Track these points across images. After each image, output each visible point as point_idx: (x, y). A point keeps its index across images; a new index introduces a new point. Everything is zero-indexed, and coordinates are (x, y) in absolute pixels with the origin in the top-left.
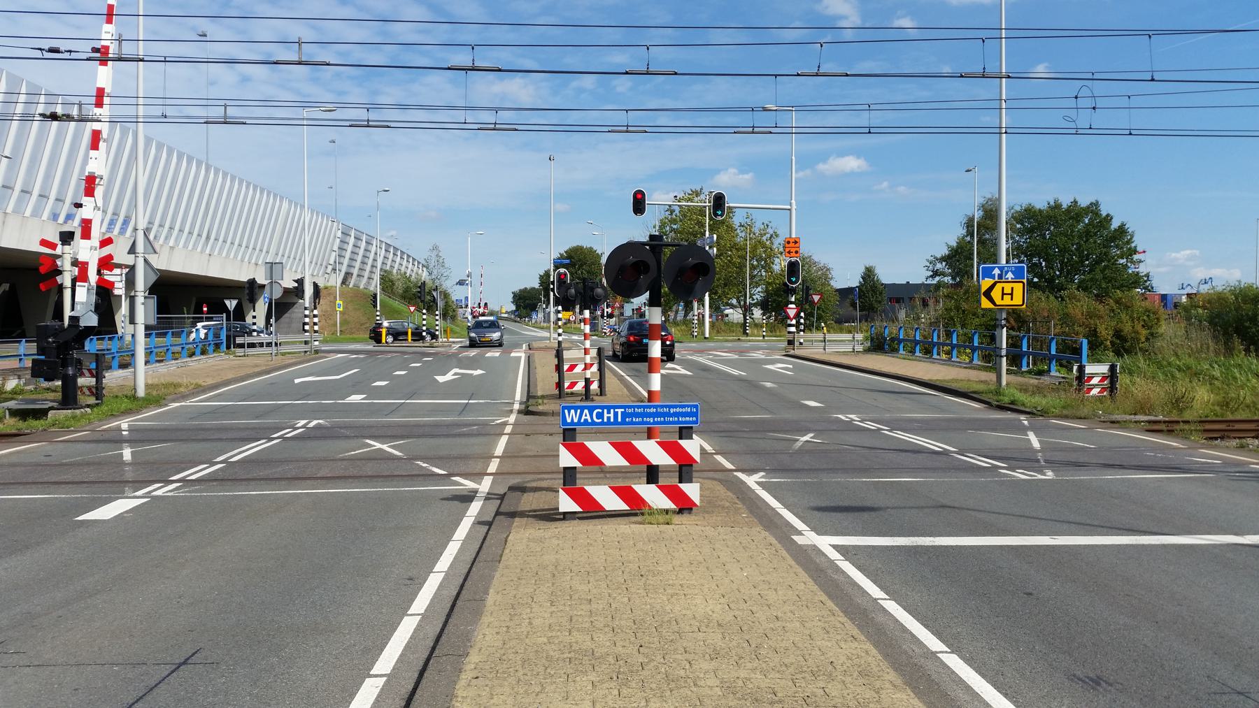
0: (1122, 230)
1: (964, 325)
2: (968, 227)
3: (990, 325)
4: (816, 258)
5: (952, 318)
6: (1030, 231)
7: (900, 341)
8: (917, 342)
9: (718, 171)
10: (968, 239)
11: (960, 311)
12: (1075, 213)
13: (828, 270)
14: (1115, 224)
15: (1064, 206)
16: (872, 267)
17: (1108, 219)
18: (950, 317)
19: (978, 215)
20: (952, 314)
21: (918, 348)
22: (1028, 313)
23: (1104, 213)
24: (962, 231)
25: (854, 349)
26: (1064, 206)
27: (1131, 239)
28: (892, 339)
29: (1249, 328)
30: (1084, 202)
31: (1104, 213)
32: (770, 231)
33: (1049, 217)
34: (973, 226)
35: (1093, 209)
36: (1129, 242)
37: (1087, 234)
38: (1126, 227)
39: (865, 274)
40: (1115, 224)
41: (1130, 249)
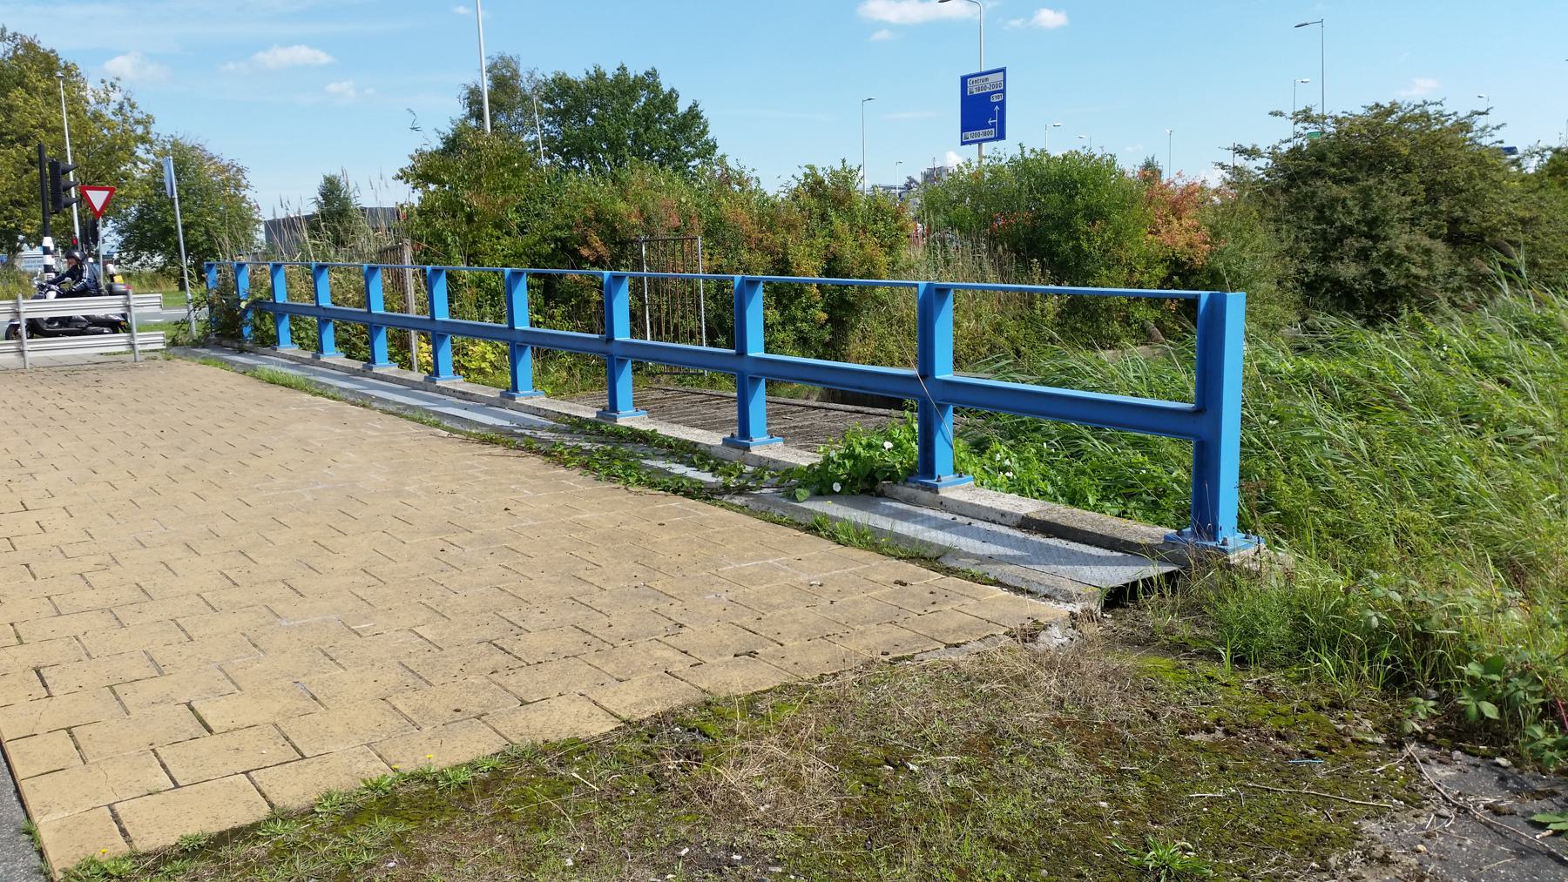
0: (693, 115)
1: (475, 254)
2: (470, 105)
3: (540, 256)
4: (213, 148)
5: (439, 237)
6: (565, 114)
7: (279, 312)
8: (324, 317)
9: (113, 54)
10: (473, 123)
11: (460, 216)
12: (625, 88)
13: (239, 170)
14: (682, 107)
15: (610, 76)
16: (335, 177)
17: (672, 97)
18: (432, 234)
19: (486, 85)
20: (439, 224)
21: (329, 336)
22: (634, 220)
23: (666, 88)
24: (460, 111)
25: (132, 345)
26: (610, 76)
27: (704, 129)
28: (258, 306)
29: (1058, 243)
30: (636, 70)
31: (666, 88)
32: (116, 97)
33: (589, 89)
34: (481, 103)
35: (649, 82)
36: (704, 132)
37: (646, 118)
38: (699, 109)
39: (324, 188)
40: (682, 107)
41: (707, 143)
